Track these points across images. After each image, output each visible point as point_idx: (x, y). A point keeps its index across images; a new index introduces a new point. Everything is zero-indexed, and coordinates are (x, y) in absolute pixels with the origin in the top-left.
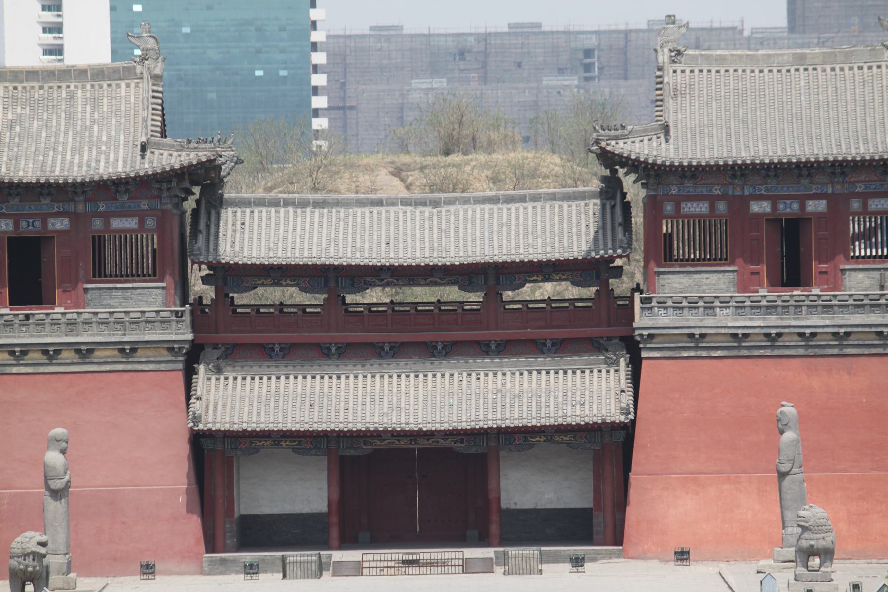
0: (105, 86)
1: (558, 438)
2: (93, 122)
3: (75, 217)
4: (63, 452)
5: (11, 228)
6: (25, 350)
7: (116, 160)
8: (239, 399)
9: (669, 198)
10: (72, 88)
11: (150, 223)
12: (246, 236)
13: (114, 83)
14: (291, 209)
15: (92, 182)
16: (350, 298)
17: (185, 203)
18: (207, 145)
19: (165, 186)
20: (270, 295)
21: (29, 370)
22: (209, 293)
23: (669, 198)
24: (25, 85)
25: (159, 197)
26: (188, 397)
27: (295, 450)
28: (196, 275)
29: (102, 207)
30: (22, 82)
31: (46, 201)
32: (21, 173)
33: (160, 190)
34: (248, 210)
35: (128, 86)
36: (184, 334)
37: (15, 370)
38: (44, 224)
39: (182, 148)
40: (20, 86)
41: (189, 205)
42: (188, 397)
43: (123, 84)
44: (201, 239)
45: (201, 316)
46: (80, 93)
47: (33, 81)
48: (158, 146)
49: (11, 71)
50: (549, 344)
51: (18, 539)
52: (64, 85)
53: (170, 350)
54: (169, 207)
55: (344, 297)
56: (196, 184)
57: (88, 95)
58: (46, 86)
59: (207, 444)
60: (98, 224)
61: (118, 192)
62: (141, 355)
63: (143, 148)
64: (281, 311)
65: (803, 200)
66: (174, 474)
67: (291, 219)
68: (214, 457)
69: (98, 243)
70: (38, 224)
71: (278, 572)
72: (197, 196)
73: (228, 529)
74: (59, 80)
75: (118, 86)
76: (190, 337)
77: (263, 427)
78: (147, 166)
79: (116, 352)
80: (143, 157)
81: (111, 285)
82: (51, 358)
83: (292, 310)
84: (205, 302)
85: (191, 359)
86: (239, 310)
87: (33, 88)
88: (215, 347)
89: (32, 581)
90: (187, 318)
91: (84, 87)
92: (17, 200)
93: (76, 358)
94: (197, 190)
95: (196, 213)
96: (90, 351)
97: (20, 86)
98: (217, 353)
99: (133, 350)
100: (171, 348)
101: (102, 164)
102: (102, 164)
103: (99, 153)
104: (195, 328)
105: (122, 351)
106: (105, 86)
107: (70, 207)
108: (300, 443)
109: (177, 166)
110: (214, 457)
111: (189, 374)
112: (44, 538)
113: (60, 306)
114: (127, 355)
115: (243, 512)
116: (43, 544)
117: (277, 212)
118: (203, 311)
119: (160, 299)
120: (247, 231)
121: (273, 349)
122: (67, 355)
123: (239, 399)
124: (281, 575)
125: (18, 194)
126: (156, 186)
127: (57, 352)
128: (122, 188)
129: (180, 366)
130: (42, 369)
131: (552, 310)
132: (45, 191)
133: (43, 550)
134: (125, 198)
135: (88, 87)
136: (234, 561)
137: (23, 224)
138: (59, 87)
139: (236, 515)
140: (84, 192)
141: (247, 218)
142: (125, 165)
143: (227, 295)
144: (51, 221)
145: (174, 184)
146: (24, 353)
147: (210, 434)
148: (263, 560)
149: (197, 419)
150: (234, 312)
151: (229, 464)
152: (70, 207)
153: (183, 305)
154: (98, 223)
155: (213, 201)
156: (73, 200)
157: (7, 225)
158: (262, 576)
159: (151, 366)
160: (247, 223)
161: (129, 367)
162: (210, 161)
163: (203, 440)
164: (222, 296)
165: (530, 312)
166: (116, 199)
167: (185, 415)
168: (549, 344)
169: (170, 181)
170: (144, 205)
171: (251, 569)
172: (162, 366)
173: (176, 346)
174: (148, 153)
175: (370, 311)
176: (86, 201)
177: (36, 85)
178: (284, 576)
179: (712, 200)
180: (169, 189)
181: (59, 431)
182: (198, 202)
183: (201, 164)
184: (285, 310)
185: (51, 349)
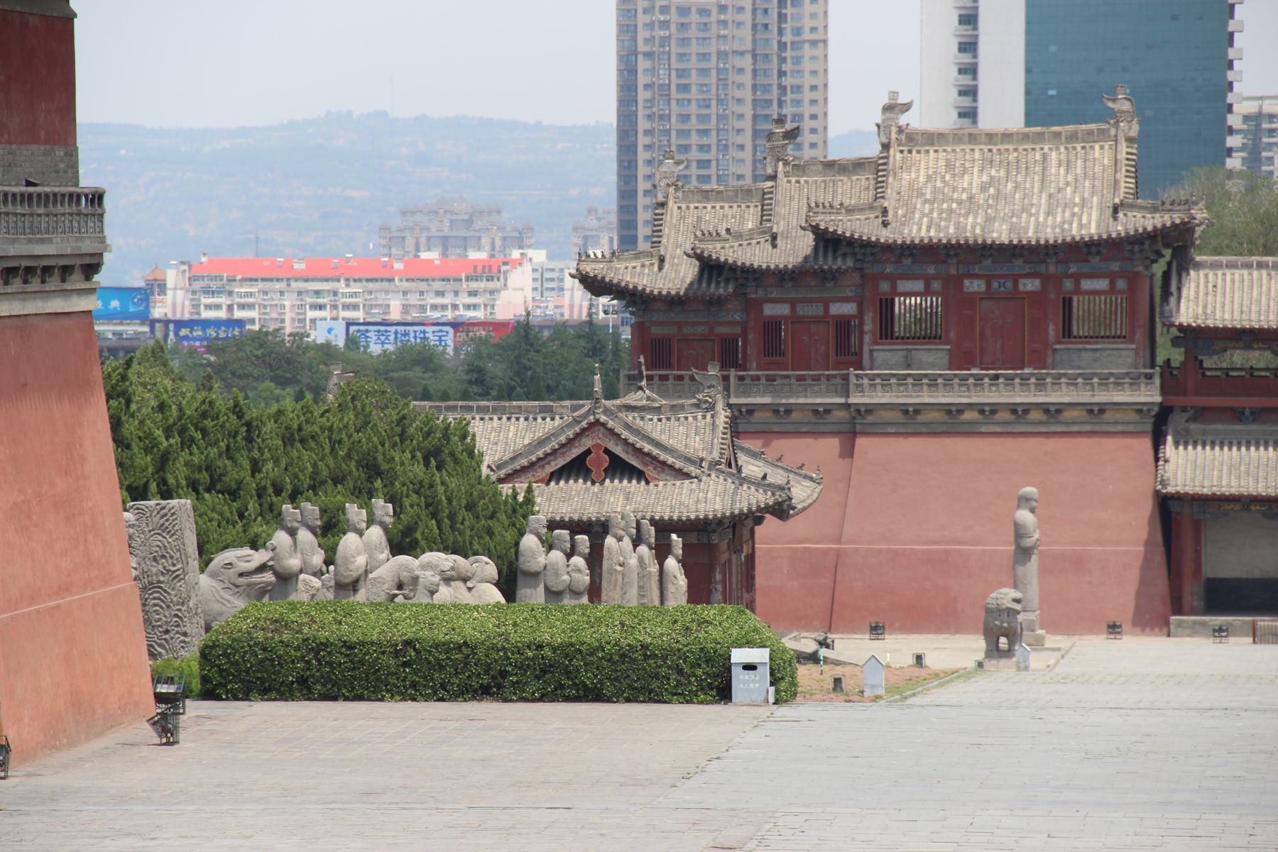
0: (1079, 149)
1: (1253, 508)
2: (1067, 184)
3: (1045, 278)
4: (1032, 510)
5: (983, 288)
6: (994, 409)
7: (1089, 222)
8: (1196, 467)
9: (885, 277)
10: (1046, 150)
11: (1121, 284)
12: (1219, 299)
13: (1088, 145)
14: (1264, 272)
15: (1064, 242)
16: (1208, 363)
17: (1155, 265)
18: (1182, 207)
19: (1137, 248)
20: (1238, 358)
21: (998, 429)
22: (1178, 357)
23: (885, 277)
24: (1000, 147)
25: (1131, 259)
26: (1157, 460)
27: (1265, 515)
28: (1162, 339)
29: (1073, 269)
30: (996, 144)
31: (1019, 262)
32: (995, 235)
33: (1132, 251)
34: (1220, 273)
35: (1102, 148)
36: (1150, 395)
37: (984, 429)
38: (1016, 285)
39: (1155, 209)
40: (995, 148)
41: (1159, 268)
42: (1157, 460)
43: (1097, 146)
44: (1173, 300)
45: (1171, 380)
46: (1054, 155)
47: (1009, 143)
48: (1132, 206)
49: (987, 134)
50: (1247, 412)
51: (993, 595)
52: (1038, 147)
53: (1139, 411)
54: (1141, 268)
55: (1201, 361)
56: (1167, 246)
57: (1062, 157)
58: (1021, 148)
59: (1175, 507)
60: (885, 286)
61: (1089, 253)
62: (1108, 416)
63: (1116, 210)
64: (1252, 375)
65: (1016, 279)
66: (1134, 528)
67: (1265, 281)
68: (1177, 518)
69: (1067, 304)
70: (1009, 285)
71: (1247, 635)
72: (1168, 258)
73: (1193, 592)
74: (1033, 142)
75: (1092, 148)
76: (1158, 399)
77: (1234, 491)
78: (1120, 228)
79: (1084, 413)
80: (1115, 219)
81: (1081, 346)
82: (1019, 417)
83: (1263, 374)
84: (1173, 364)
85: (1159, 426)
86: (1208, 373)
87: (1007, 150)
88: (1184, 410)
89: (1006, 636)
90: (1157, 381)
91: (1058, 149)
92: (989, 261)
93: (1044, 417)
94: (1168, 253)
95: (1166, 276)
96: (1059, 411)
97: (995, 148)
98: (1185, 416)
99: (1102, 411)
100: (1139, 409)
101: (1075, 225)
102: (1075, 225)
103: (1074, 215)
104: (1164, 390)
105: (1091, 412)
106: (1079, 149)
107: (1041, 268)
108: (1270, 508)
109: (1150, 228)
110: (1177, 518)
111: (1158, 442)
112: (1018, 595)
113: (1030, 366)
114: (1052, 417)
115: (1211, 575)
116: (1017, 601)
117: (1250, 274)
118: (1171, 374)
119: (1130, 360)
120: (1219, 294)
121: (1243, 413)
122: (1004, 416)
123: (1196, 467)
124: (1251, 639)
125: (991, 255)
126: (1128, 247)
127: (1026, 412)
128: (1094, 249)
129: (1149, 428)
130: (1010, 429)
131: (1250, 381)
132: (907, 252)
133: (1018, 607)
134: (1097, 259)
135: (1062, 149)
136: (1203, 624)
137: (995, 285)
138: (972, 150)
139: (1204, 578)
140: (1056, 254)
141: (1219, 281)
142: (1098, 227)
143: (1196, 358)
144: (1022, 281)
145: (1147, 246)
146: (993, 412)
147: (1178, 497)
148: (1230, 624)
149: (1164, 483)
150: (1203, 374)
151: (1197, 526)
152: (1041, 268)
153: (1153, 366)
154: (1068, 284)
155: (1182, 262)
156: (1044, 261)
157: (979, 286)
158: (1232, 640)
159: (1119, 428)
160: (1219, 286)
161: (1097, 428)
162: (1184, 223)
163: (1171, 502)
164: (1193, 360)
165: (1228, 382)
166: (1087, 261)
167: (1153, 477)
168: (1247, 412)
169: (1142, 243)
170: (1115, 267)
171: (1219, 632)
172: (1131, 428)
173: (1145, 408)
174: (1121, 215)
175: (1227, 375)
176: (958, 263)
177: (1011, 147)
178: (1254, 642)
179: (1113, 278)
180: (1141, 251)
181: (1030, 490)
182: (1169, 264)
183: (1174, 225)
184: (1256, 373)
185: (987, 408)
